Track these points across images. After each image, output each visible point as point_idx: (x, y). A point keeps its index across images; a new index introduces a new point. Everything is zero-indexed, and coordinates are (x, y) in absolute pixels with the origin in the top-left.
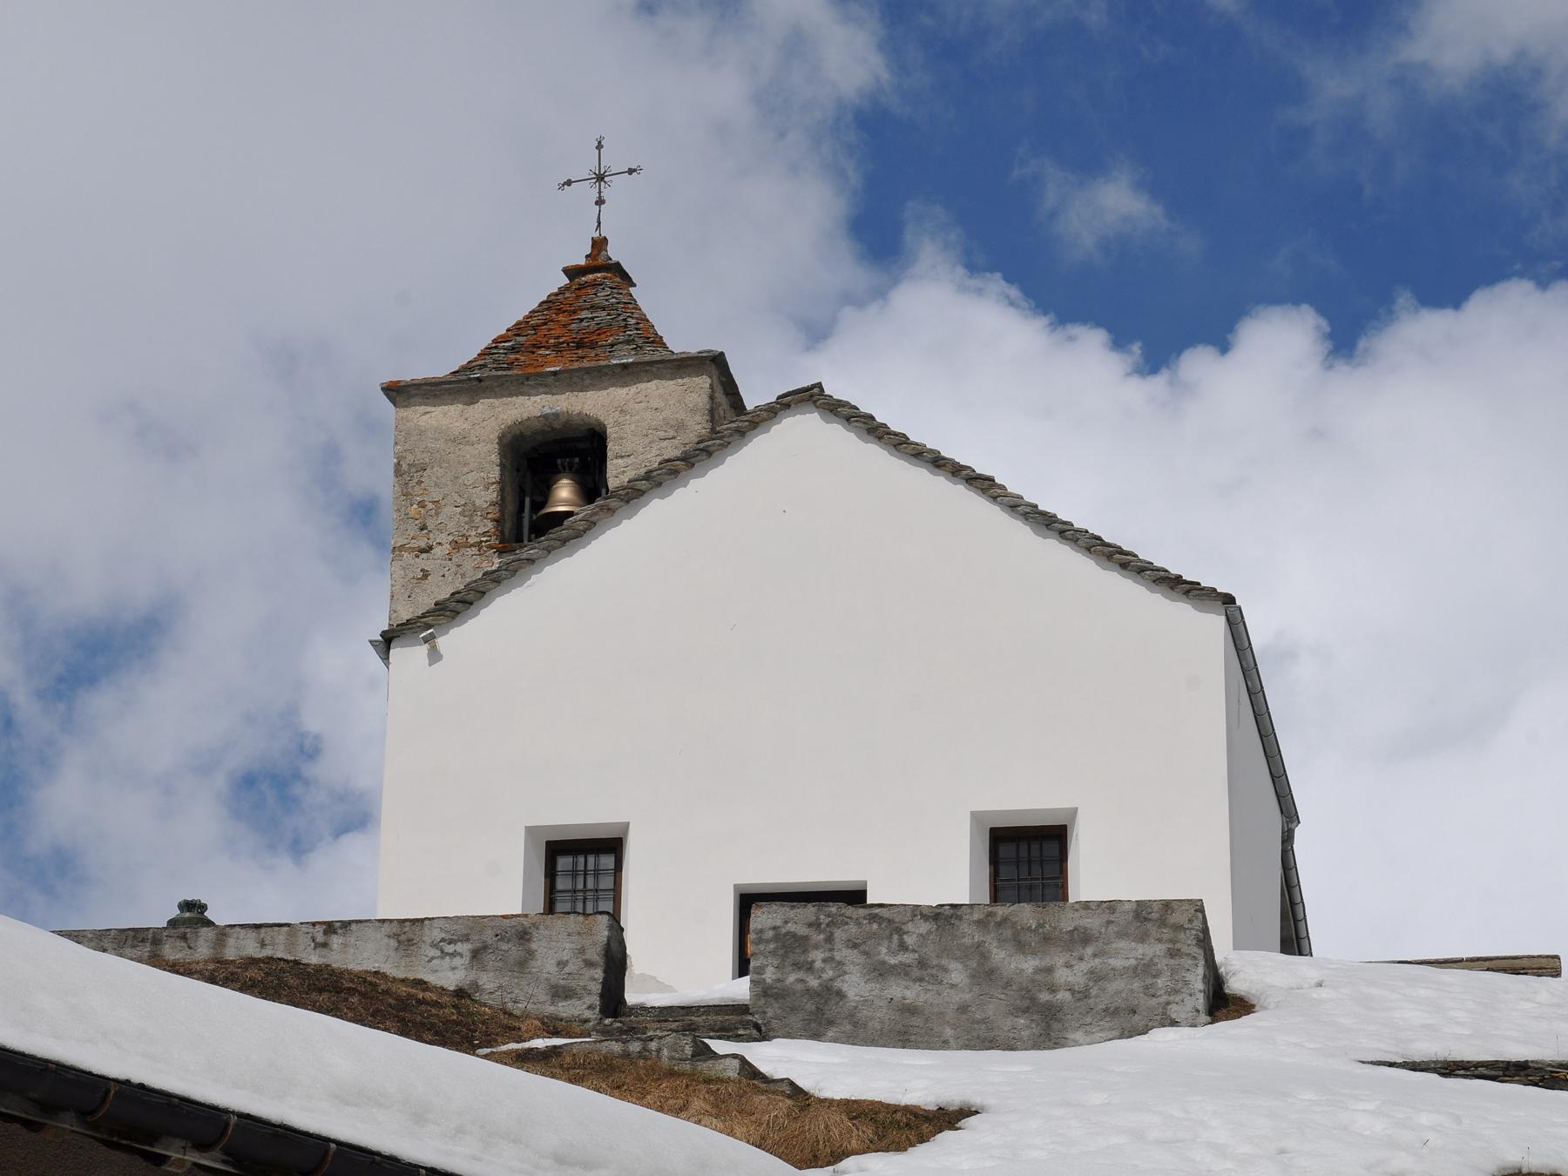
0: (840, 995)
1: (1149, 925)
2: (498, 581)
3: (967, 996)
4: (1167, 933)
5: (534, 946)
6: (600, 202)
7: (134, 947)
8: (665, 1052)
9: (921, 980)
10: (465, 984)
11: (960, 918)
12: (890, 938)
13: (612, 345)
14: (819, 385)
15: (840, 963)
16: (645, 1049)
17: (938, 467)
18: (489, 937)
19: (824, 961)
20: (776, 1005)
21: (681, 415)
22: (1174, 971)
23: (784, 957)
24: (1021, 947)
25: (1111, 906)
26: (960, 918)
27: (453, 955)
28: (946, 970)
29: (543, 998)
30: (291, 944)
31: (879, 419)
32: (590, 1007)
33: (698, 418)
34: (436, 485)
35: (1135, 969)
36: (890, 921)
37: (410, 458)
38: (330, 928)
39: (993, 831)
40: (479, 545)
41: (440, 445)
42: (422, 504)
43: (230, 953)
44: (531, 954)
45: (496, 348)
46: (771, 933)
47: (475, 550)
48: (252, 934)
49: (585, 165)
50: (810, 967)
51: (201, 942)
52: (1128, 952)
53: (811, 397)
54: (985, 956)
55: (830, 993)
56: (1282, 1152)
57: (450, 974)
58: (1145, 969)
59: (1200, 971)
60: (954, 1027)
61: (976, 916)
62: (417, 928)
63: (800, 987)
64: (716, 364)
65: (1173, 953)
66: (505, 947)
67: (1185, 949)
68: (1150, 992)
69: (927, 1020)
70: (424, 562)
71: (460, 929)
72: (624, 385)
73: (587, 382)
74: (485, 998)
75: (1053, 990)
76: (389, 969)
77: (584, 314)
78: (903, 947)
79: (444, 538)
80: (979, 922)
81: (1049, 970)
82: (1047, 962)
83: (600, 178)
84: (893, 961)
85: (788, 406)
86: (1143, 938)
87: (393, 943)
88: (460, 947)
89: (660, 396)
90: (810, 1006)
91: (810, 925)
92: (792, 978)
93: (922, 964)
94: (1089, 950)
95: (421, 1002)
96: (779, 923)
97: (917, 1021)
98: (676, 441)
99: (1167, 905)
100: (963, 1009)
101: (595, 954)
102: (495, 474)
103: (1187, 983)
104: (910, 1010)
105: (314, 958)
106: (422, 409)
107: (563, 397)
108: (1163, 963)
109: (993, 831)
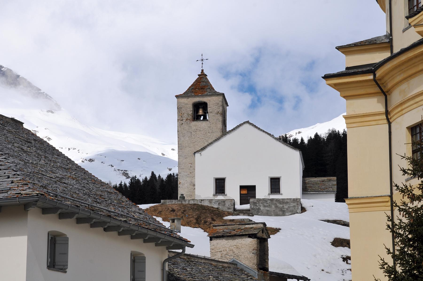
0: (260, 209)
1: (294, 201)
2: (208, 146)
3: (274, 209)
4: (297, 202)
5: (225, 203)
6: (202, 64)
7: (179, 202)
8: (246, 220)
9: (269, 207)
10: (218, 207)
11: (273, 200)
12: (266, 202)
13: (207, 89)
14: (249, 121)
15: (260, 205)
16: (243, 220)
17: (264, 132)
18: (220, 202)
19: (258, 205)
20: (253, 210)
21: (218, 102)
22: (297, 207)
23: (254, 205)
24: (280, 203)
25: (290, 199)
26: (273, 200)
27: (216, 204)
28: (272, 206)
29: (227, 209)
30: (197, 202)
31: (256, 126)
32: (232, 210)
33: (221, 103)
34: (183, 111)
35: (293, 206)
36: (266, 200)
37: (179, 107)
38: (202, 200)
39: (271, 178)
40: (190, 120)
41: (183, 105)
42: (181, 113)
43: (190, 203)
44: (225, 204)
45: (190, 88)
46: (252, 202)
47: (189, 120)
48: (192, 201)
49: (200, 58)
50: (257, 206)
51: (187, 201)
52: (292, 204)
53: (248, 122)
54: (276, 205)
55: (259, 209)
56: (313, 236)
57: (216, 206)
58: (294, 206)
59: (300, 206)
60: (273, 213)
61: (275, 200)
62: (212, 200)
63: (256, 208)
64: (223, 95)
65: (297, 205)
66: (222, 203)
67: (299, 204)
68: (295, 209)
69: (270, 212)
70: (182, 122)
71: (217, 201)
72: (210, 97)
73: (204, 96)
74: (220, 209)
75: (284, 208)
76: (209, 205)
77: (202, 83)
78: (267, 203)
79: (185, 118)
80: (276, 201)
81: (284, 206)
82: (283, 205)
83: (202, 60)
84: (266, 205)
85: (245, 123)
86: (294, 203)
87: (209, 202)
88: (217, 203)
89: (215, 99)
90: (257, 210)
91: (257, 201)
92: (255, 207)
93: (269, 205)
94: (288, 204)
95: (214, 210)
96: (253, 201)
97: (269, 212)
98: (217, 106)
99: (297, 199)
100: (274, 211)
101: (232, 204)
102: (192, 109)
103: (299, 208)
104: (268, 211)
105: (200, 204)
106: (181, 99)
107: (201, 98)
108: (296, 206)
109: (271, 178)
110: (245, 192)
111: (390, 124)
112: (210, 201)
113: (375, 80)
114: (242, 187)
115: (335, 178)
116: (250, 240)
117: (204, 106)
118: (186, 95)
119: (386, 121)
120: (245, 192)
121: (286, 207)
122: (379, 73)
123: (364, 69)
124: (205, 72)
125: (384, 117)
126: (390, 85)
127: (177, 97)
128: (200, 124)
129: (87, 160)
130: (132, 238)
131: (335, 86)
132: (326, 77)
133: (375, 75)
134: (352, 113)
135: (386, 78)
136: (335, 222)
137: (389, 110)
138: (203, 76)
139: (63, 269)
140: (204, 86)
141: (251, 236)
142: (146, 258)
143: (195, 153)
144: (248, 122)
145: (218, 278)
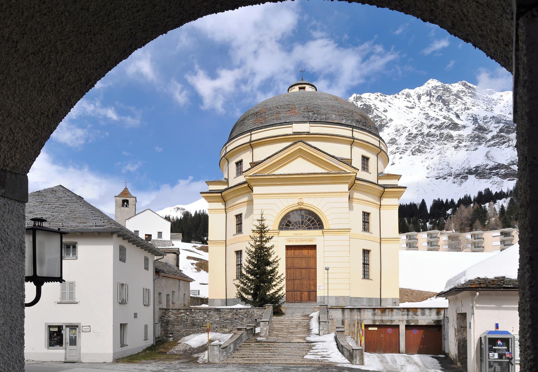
52: (169, 243)
53: (149, 209)
110: (147, 237)
111: (226, 213)
113: (221, 196)
115: (181, 234)
116: (173, 254)
117: (127, 201)
118: (119, 196)
119: (225, 212)
120: (147, 237)
121: (166, 243)
122: (223, 193)
124: (127, 188)
125: (224, 211)
126: (227, 199)
127: (115, 196)
128: (125, 208)
131: (205, 197)
132: (201, 193)
133: (222, 194)
134: (211, 208)
135: (226, 196)
136: (186, 250)
137: (226, 208)
138: (126, 189)
141: (173, 253)
144: (149, 209)
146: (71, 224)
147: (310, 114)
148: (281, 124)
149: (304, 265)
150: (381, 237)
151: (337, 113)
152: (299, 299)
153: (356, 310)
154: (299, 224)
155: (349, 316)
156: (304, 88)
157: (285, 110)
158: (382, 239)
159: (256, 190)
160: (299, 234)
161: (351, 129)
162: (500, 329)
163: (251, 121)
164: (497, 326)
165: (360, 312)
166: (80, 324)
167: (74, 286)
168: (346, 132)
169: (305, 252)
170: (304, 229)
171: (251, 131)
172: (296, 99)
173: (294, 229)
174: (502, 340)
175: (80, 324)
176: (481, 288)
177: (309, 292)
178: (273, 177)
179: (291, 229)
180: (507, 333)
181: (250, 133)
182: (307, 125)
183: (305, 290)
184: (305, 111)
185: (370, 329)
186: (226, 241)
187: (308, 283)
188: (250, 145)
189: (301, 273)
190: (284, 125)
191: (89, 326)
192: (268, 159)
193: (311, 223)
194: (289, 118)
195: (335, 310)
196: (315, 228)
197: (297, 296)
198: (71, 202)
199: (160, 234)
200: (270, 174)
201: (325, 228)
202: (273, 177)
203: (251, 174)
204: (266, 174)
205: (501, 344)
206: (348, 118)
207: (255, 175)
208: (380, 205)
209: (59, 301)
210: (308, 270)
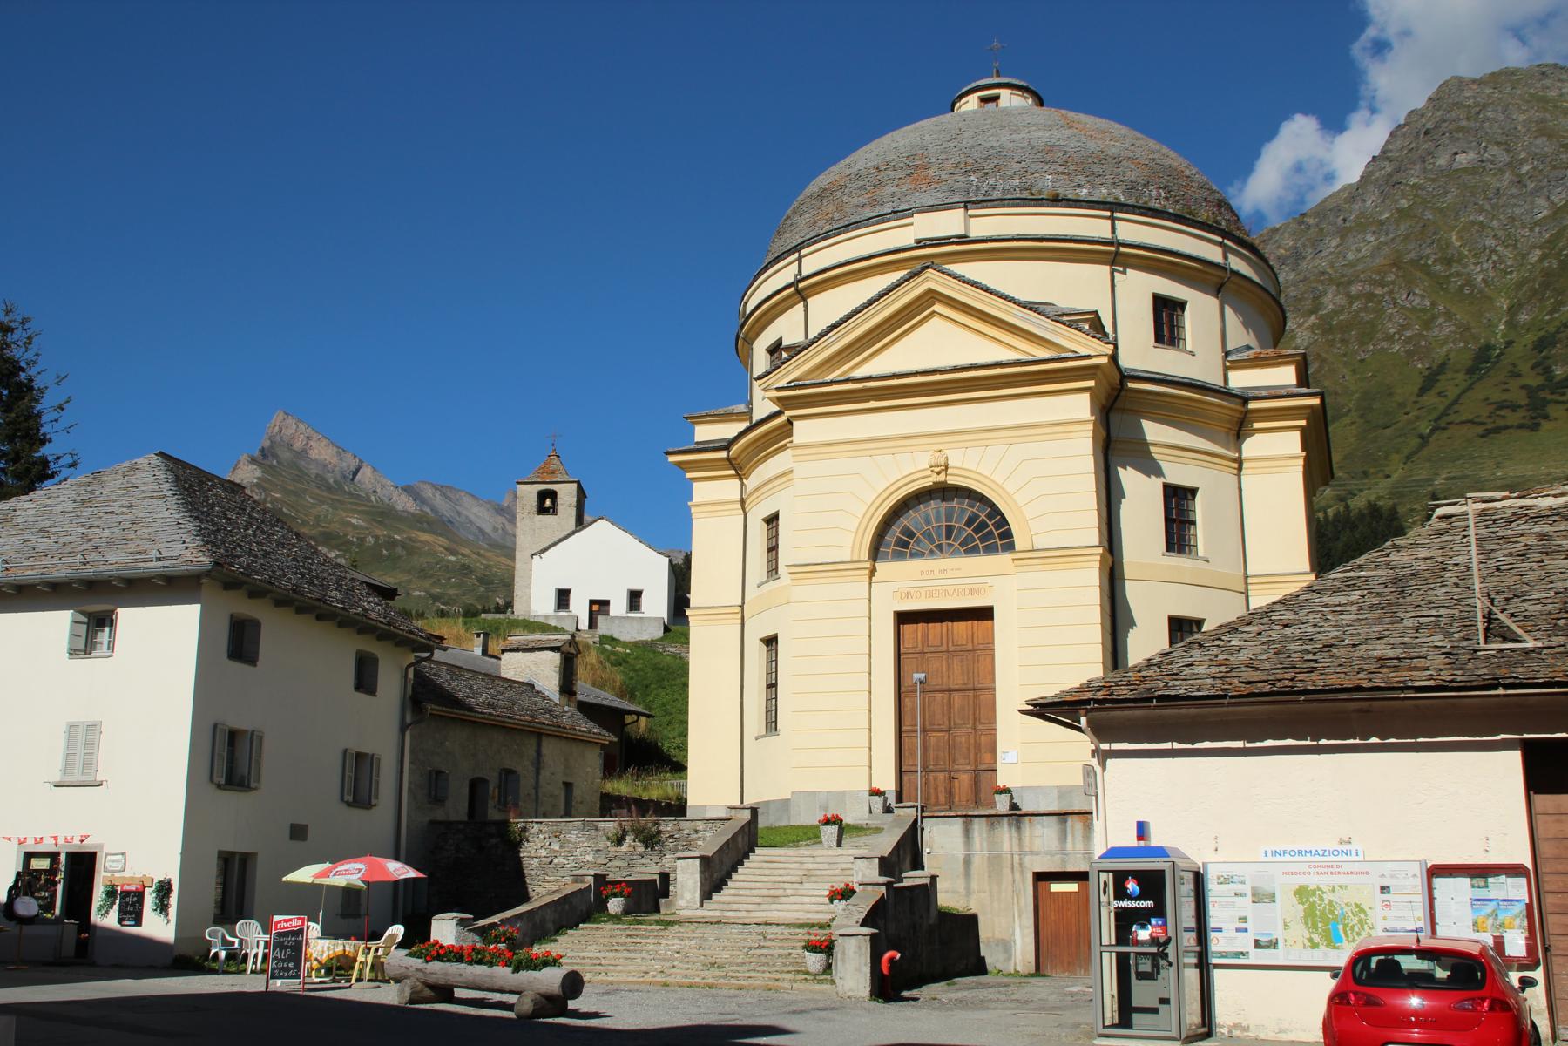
112: (547, 617)
114: (592, 602)
117: (552, 495)
123: (716, 445)
129: (1340, 887)
130: (319, 618)
139: (252, 661)
140: (555, 470)
141: (553, 649)
142: (262, 626)
143: (533, 555)
145: (575, 730)
146: (112, 556)
147: (972, 178)
148: (883, 218)
149: (957, 681)
150: (1249, 573)
151: (1060, 169)
152: (942, 799)
153: (1006, 819)
154: (939, 536)
155: (985, 844)
156: (996, 98)
157: (898, 174)
158: (1250, 580)
159: (804, 431)
160: (936, 572)
161: (1108, 214)
162: (1155, 840)
163: (808, 215)
164: (1142, 830)
165: (1018, 828)
166: (101, 846)
167: (98, 734)
168: (1094, 226)
169: (960, 628)
170: (954, 553)
171: (796, 249)
172: (934, 136)
173: (923, 554)
174: (1140, 876)
175: (101, 846)
176: (1096, 701)
177: (977, 771)
178: (850, 386)
179: (913, 555)
180: (1160, 852)
181: (796, 256)
182: (959, 213)
183: (961, 768)
184: (958, 170)
185: (1056, 887)
186: (742, 606)
187: (972, 741)
188: (797, 290)
189: (950, 705)
190: (889, 220)
191: (123, 854)
192: (831, 330)
193: (976, 531)
194: (908, 198)
195: (945, 824)
196: (991, 549)
197: (936, 788)
198: (152, 498)
199: (635, 598)
200: (842, 378)
201: (1017, 547)
202: (850, 386)
203: (782, 383)
204: (828, 378)
205: (1137, 890)
206: (1098, 181)
207: (792, 384)
208: (1240, 462)
209: (58, 778)
210: (971, 694)
